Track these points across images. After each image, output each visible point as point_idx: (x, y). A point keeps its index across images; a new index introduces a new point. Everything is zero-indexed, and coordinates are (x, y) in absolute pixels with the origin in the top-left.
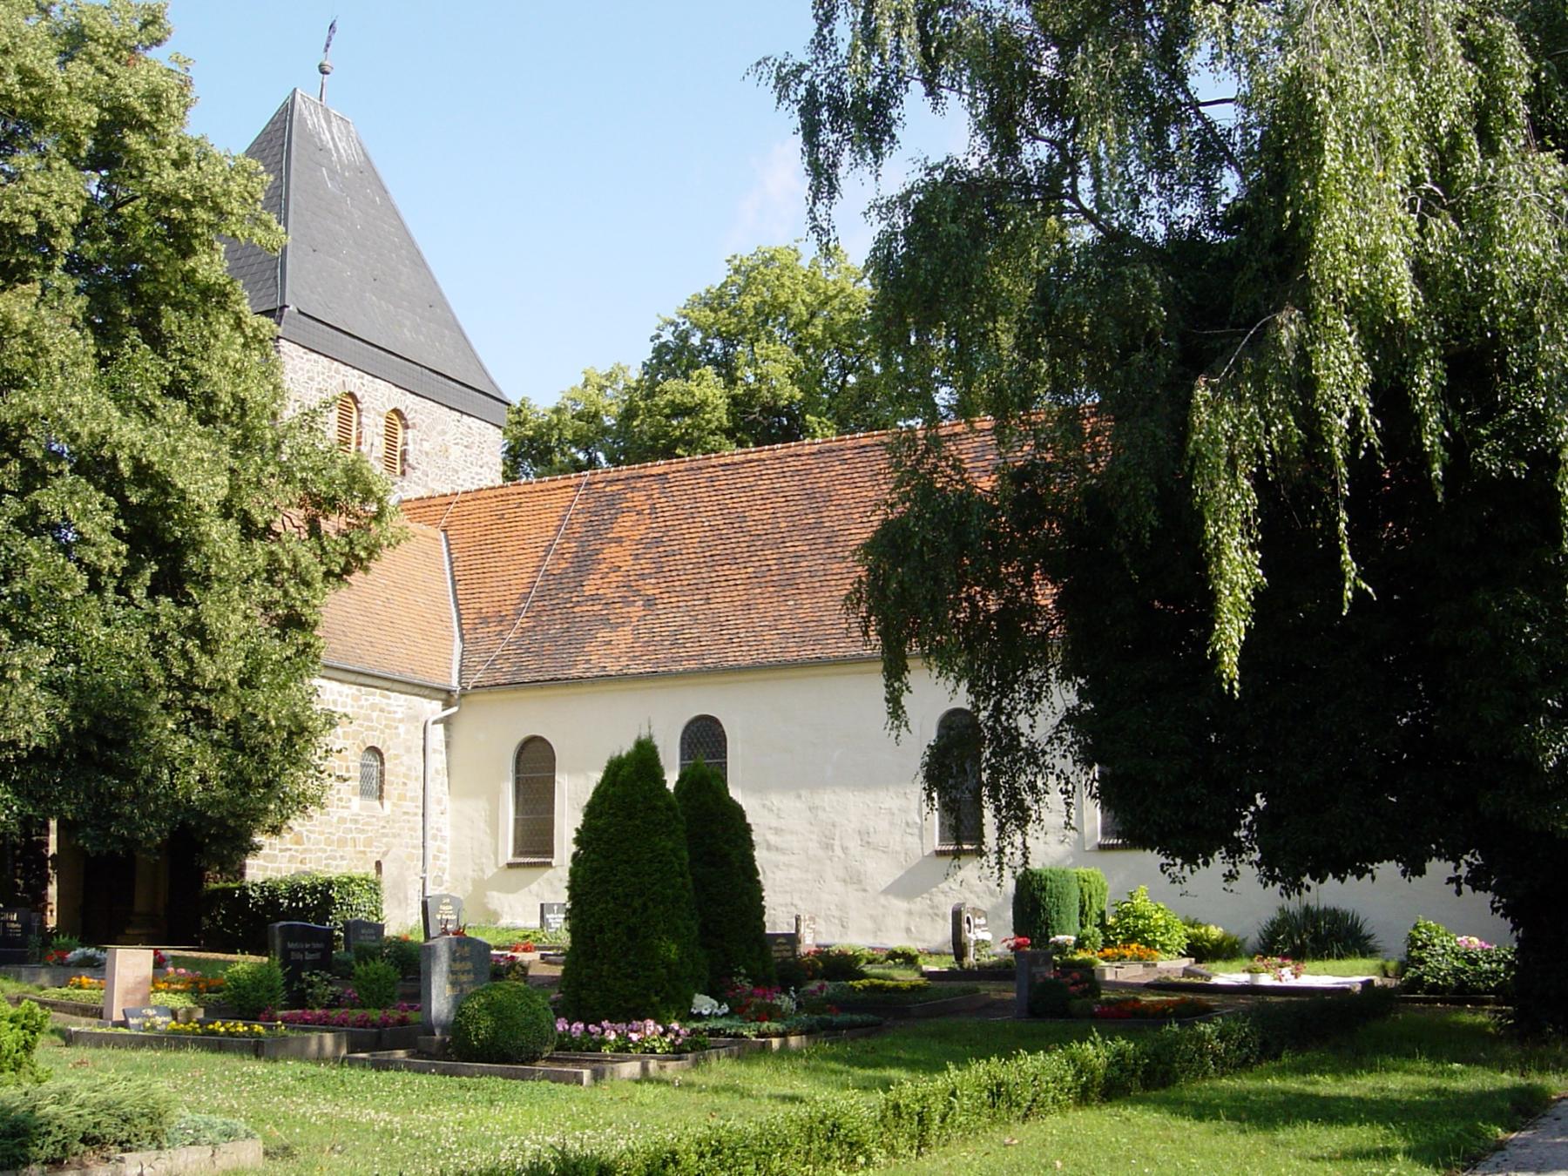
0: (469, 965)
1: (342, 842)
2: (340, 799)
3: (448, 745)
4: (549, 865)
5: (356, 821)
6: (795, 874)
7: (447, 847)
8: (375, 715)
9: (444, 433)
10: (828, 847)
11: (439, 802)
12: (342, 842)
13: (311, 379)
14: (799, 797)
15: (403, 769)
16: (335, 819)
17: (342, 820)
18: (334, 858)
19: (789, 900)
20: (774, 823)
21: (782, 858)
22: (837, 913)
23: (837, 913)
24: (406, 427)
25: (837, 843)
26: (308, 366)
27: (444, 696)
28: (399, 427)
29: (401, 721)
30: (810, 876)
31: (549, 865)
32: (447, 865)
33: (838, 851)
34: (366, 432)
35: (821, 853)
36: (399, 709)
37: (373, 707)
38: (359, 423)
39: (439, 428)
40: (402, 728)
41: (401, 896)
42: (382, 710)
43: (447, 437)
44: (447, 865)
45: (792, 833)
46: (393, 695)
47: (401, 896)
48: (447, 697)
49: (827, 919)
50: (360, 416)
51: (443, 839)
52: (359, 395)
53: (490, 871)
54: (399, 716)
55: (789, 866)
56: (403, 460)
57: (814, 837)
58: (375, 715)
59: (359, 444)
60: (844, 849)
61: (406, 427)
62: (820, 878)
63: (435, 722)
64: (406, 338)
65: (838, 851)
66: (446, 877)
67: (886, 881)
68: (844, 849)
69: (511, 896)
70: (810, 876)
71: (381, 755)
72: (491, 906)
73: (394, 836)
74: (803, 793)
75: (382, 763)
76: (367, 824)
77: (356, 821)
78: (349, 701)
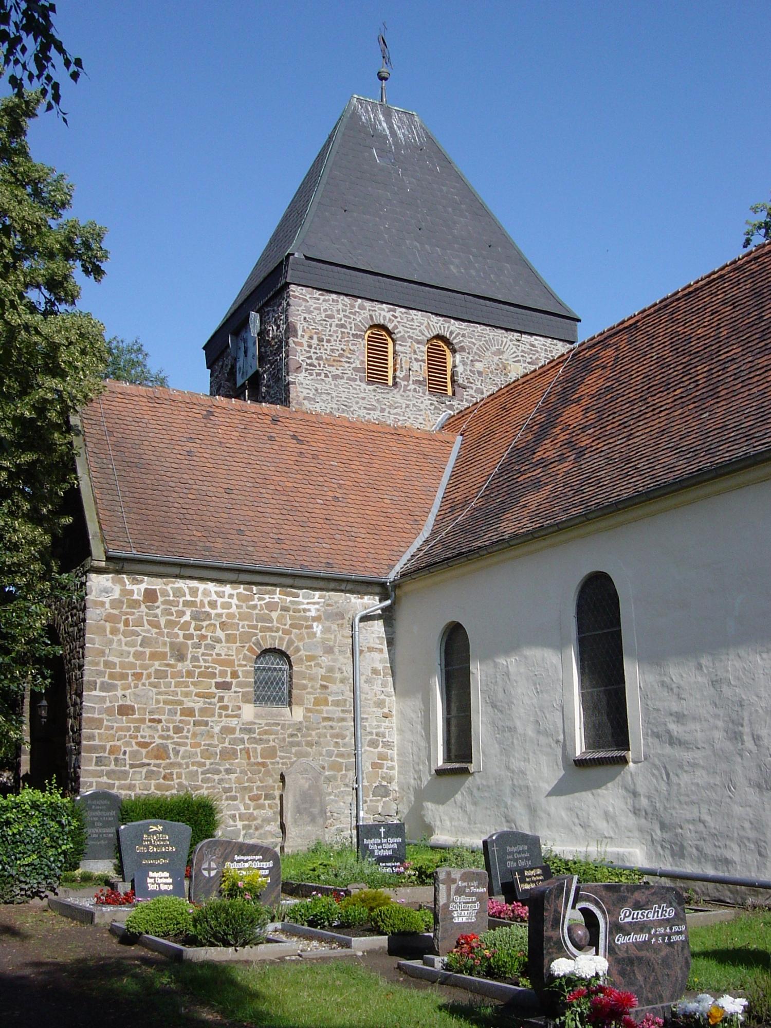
0: (541, 877)
1: (228, 754)
2: (225, 708)
3: (391, 642)
4: (465, 771)
5: (250, 731)
6: (701, 777)
7: (394, 753)
8: (274, 615)
9: (500, 352)
10: (736, 737)
11: (380, 704)
12: (228, 754)
13: (331, 317)
14: (700, 667)
15: (322, 672)
16: (217, 729)
17: (227, 730)
18: (218, 772)
19: (696, 815)
20: (675, 707)
21: (688, 756)
22: (752, 834)
23: (752, 834)
24: (454, 351)
25: (746, 729)
26: (325, 306)
27: (377, 589)
28: (448, 353)
29: (315, 619)
30: (718, 780)
31: (465, 771)
32: (395, 773)
33: (747, 739)
34: (403, 359)
35: (728, 746)
36: (312, 607)
37: (271, 606)
38: (395, 352)
39: (494, 349)
40: (317, 628)
41: (315, 811)
42: (285, 609)
43: (505, 356)
44: (395, 773)
45: (694, 719)
46: (301, 592)
47: (315, 811)
48: (383, 590)
49: (741, 841)
50: (394, 345)
51: (387, 745)
52: (390, 326)
53: (426, 779)
54: (313, 613)
55: (694, 765)
56: (453, 381)
57: (720, 724)
58: (274, 615)
59: (395, 370)
60: (756, 739)
61: (454, 351)
62: (730, 784)
63: (365, 618)
64: (455, 272)
65: (749, 744)
66: (394, 786)
67: (548, 788)
68: (756, 739)
69: (441, 808)
70: (718, 780)
71: (288, 657)
72: (427, 820)
73: (309, 744)
74: (705, 661)
75: (291, 666)
76: (266, 732)
77: (250, 731)
78: (234, 601)
